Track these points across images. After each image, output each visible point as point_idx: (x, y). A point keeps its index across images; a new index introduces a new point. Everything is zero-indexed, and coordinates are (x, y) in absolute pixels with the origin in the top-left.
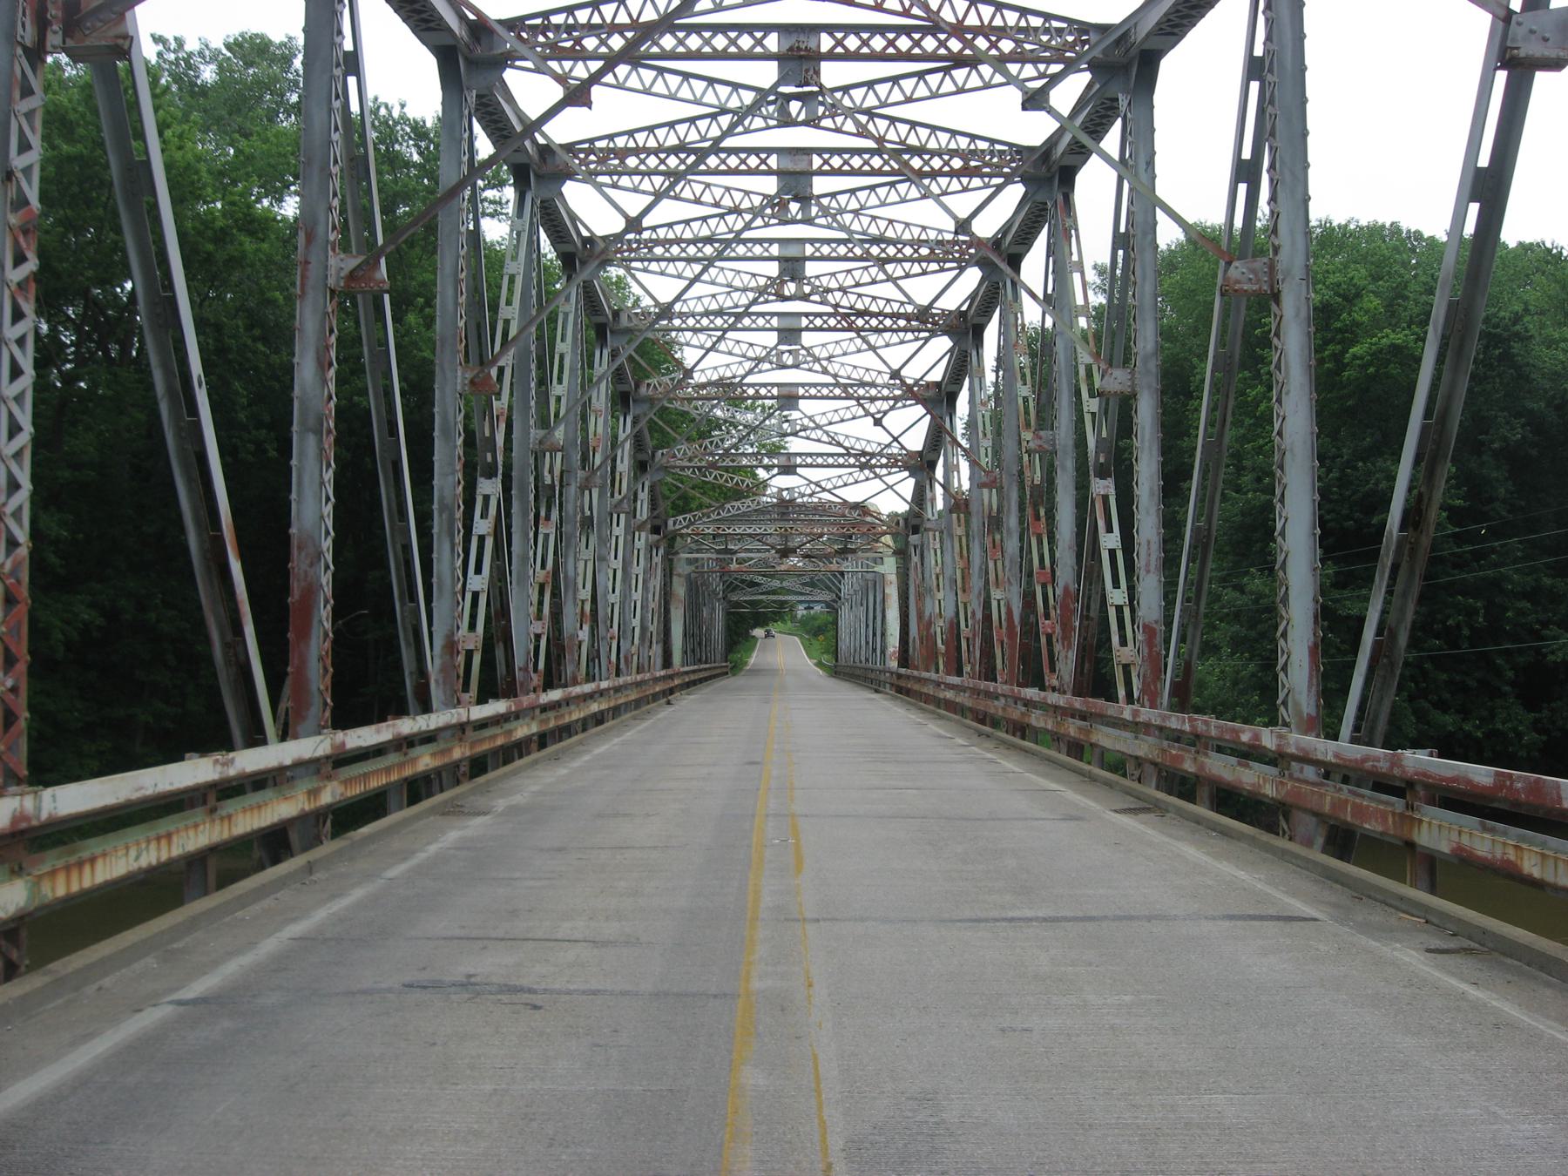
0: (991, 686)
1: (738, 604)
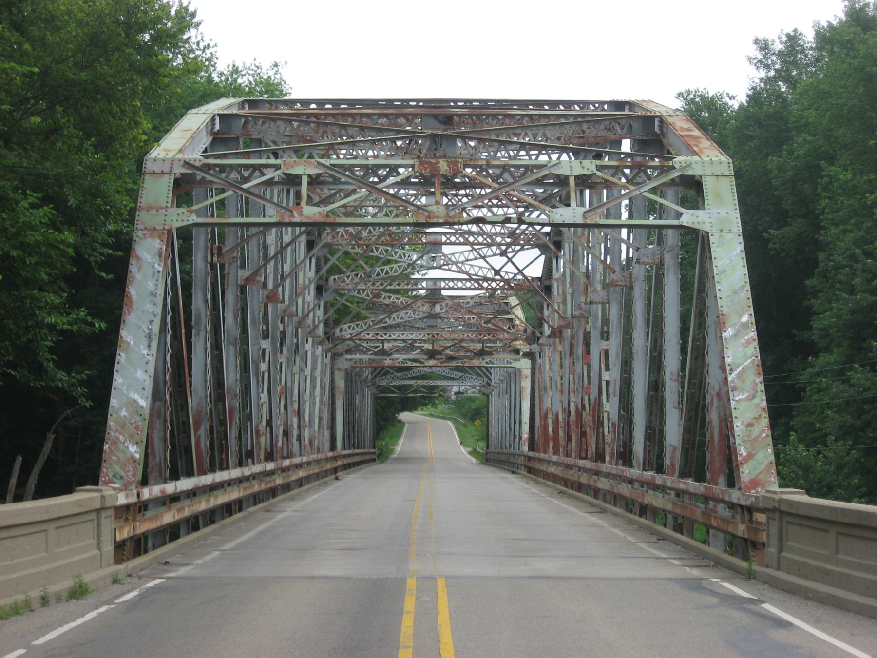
0: (659, 479)
1: (386, 390)
